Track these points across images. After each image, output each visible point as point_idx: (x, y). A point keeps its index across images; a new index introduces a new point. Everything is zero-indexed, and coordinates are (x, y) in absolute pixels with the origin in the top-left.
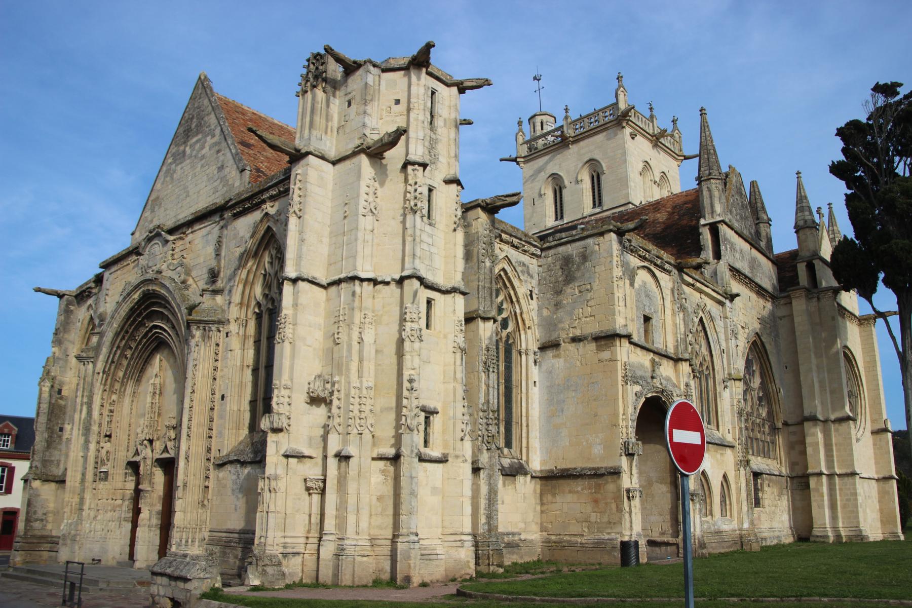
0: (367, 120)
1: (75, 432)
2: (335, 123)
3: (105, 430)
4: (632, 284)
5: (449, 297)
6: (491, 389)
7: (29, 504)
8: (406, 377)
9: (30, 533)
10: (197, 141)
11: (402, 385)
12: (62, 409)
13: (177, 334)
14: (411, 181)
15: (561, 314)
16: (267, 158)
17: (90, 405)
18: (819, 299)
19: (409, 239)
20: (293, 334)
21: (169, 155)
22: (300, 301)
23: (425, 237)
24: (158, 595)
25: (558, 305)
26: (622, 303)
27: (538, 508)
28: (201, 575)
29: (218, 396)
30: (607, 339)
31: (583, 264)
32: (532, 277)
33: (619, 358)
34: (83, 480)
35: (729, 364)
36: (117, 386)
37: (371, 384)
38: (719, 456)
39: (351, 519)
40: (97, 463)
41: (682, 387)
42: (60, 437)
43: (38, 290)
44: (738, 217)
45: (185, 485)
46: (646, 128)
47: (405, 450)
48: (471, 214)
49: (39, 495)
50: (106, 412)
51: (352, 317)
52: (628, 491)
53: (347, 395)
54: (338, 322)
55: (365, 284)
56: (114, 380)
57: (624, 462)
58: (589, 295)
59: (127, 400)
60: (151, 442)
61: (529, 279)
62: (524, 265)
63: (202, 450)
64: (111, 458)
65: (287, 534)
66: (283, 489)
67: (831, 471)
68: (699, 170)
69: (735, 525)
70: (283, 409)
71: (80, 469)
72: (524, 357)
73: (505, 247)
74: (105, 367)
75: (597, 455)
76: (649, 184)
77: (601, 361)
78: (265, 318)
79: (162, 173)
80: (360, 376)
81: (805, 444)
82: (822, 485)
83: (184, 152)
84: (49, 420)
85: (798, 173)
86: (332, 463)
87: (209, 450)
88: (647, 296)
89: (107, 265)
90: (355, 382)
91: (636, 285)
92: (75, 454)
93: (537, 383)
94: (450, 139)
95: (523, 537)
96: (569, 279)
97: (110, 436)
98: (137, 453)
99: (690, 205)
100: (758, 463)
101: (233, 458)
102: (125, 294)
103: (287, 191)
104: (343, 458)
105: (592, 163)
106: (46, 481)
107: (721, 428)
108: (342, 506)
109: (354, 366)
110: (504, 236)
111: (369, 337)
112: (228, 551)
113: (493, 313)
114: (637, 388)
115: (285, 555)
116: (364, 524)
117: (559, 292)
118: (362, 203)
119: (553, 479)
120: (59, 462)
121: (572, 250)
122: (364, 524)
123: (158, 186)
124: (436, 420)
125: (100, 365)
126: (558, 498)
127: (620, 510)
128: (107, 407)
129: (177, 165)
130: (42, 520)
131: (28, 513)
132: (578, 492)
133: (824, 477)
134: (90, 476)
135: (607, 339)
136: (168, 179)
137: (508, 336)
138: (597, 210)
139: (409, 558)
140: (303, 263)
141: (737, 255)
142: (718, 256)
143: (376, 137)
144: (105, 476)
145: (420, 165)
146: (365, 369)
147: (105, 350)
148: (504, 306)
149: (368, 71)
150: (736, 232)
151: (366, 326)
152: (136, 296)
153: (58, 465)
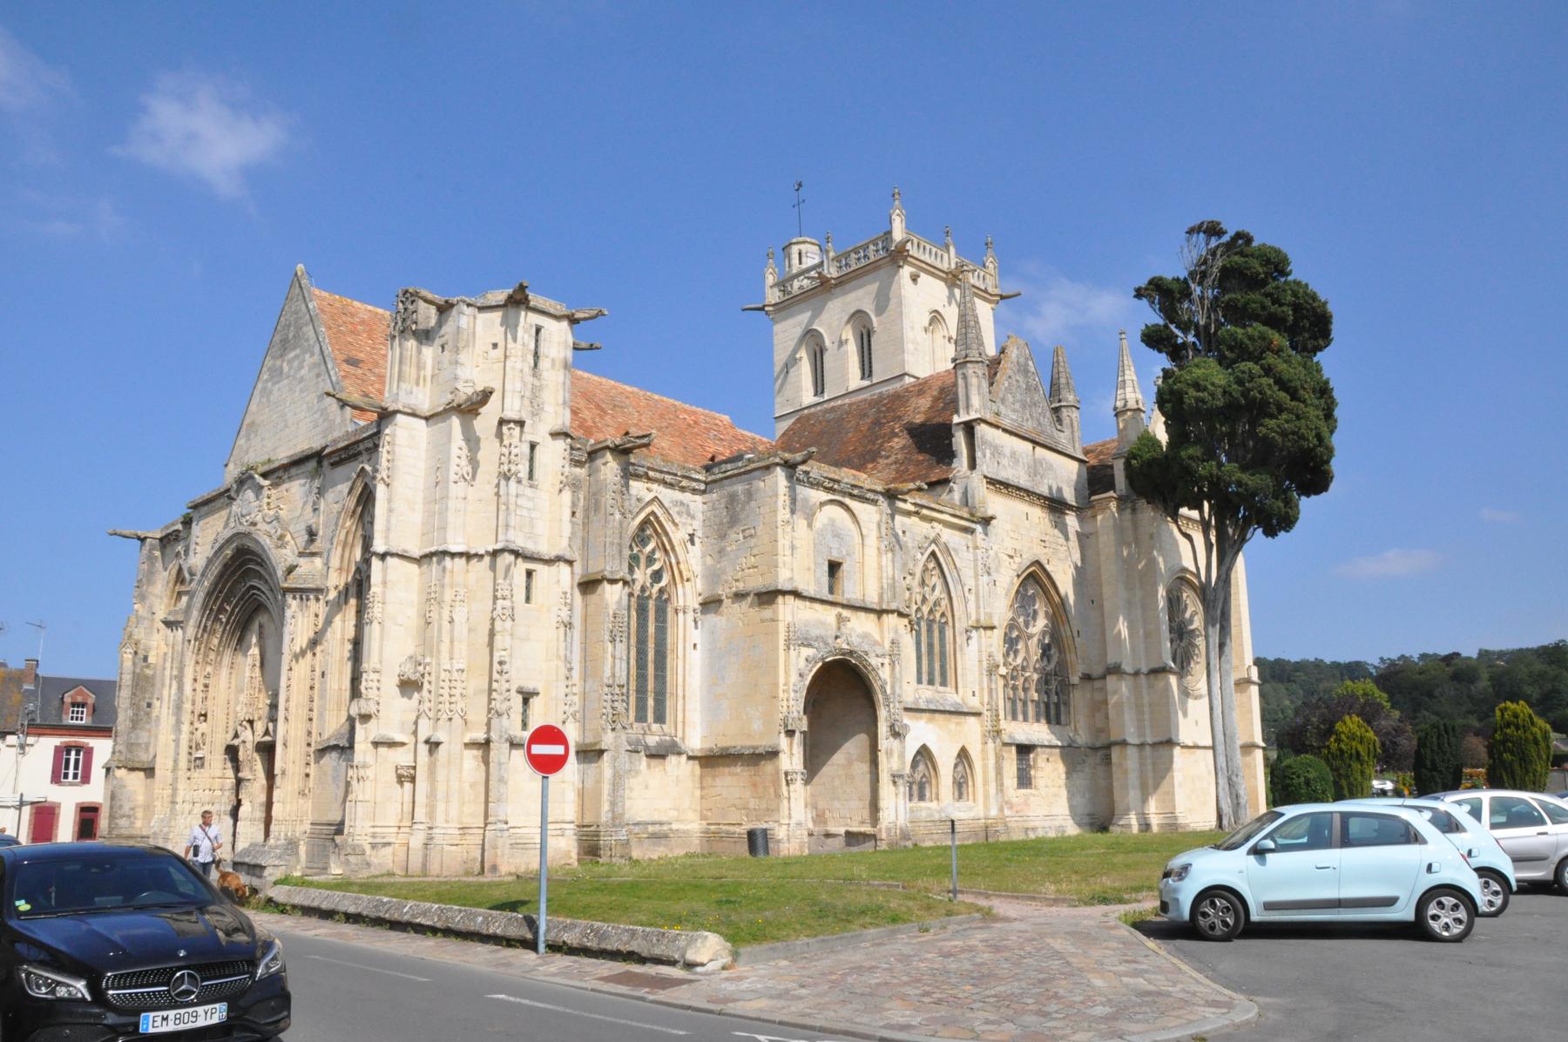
0: (459, 372)
1: (165, 711)
2: (429, 371)
3: (199, 709)
4: (810, 525)
5: (554, 569)
7: (113, 797)
8: (496, 659)
9: (115, 832)
10: (296, 357)
11: (495, 669)
12: (150, 680)
14: (506, 442)
15: (725, 563)
17: (180, 679)
19: (503, 507)
22: (389, 577)
25: (721, 552)
26: (788, 552)
27: (698, 793)
29: (318, 673)
30: (768, 597)
32: (693, 517)
33: (781, 617)
34: (175, 768)
36: (212, 656)
37: (461, 666)
41: (887, 645)
42: (148, 714)
44: (1017, 406)
45: (283, 773)
46: (938, 264)
47: (494, 736)
48: (599, 462)
50: (200, 687)
51: (442, 594)
52: (786, 774)
53: (438, 678)
54: (431, 599)
55: (457, 560)
57: (783, 742)
58: (753, 542)
59: (224, 671)
60: (251, 722)
61: (689, 521)
62: (682, 503)
63: (302, 734)
64: (208, 741)
66: (372, 777)
69: (979, 811)
70: (372, 694)
71: (172, 754)
72: (681, 615)
73: (655, 486)
75: (756, 735)
83: (281, 368)
84: (134, 694)
86: (423, 749)
87: (310, 733)
89: (195, 507)
92: (165, 740)
95: (674, 827)
96: (734, 521)
97: (205, 715)
98: (236, 736)
101: (333, 742)
102: (217, 546)
103: (376, 446)
104: (434, 746)
105: (858, 317)
106: (132, 769)
108: (432, 795)
110: (651, 474)
111: (459, 617)
113: (623, 572)
114: (810, 652)
115: (374, 846)
116: (454, 812)
117: (723, 536)
118: (454, 468)
119: (712, 760)
120: (147, 745)
121: (739, 488)
122: (454, 812)
124: (534, 701)
125: (191, 631)
126: (718, 782)
127: (778, 796)
128: (201, 681)
131: (111, 807)
134: (183, 763)
135: (768, 597)
137: (661, 591)
138: (866, 383)
139: (495, 847)
140: (392, 536)
141: (1005, 461)
142: (973, 465)
143: (470, 391)
144: (200, 763)
145: (516, 422)
146: (456, 650)
147: (195, 614)
148: (657, 555)
149: (461, 313)
150: (1005, 430)
152: (229, 552)
153: (147, 749)
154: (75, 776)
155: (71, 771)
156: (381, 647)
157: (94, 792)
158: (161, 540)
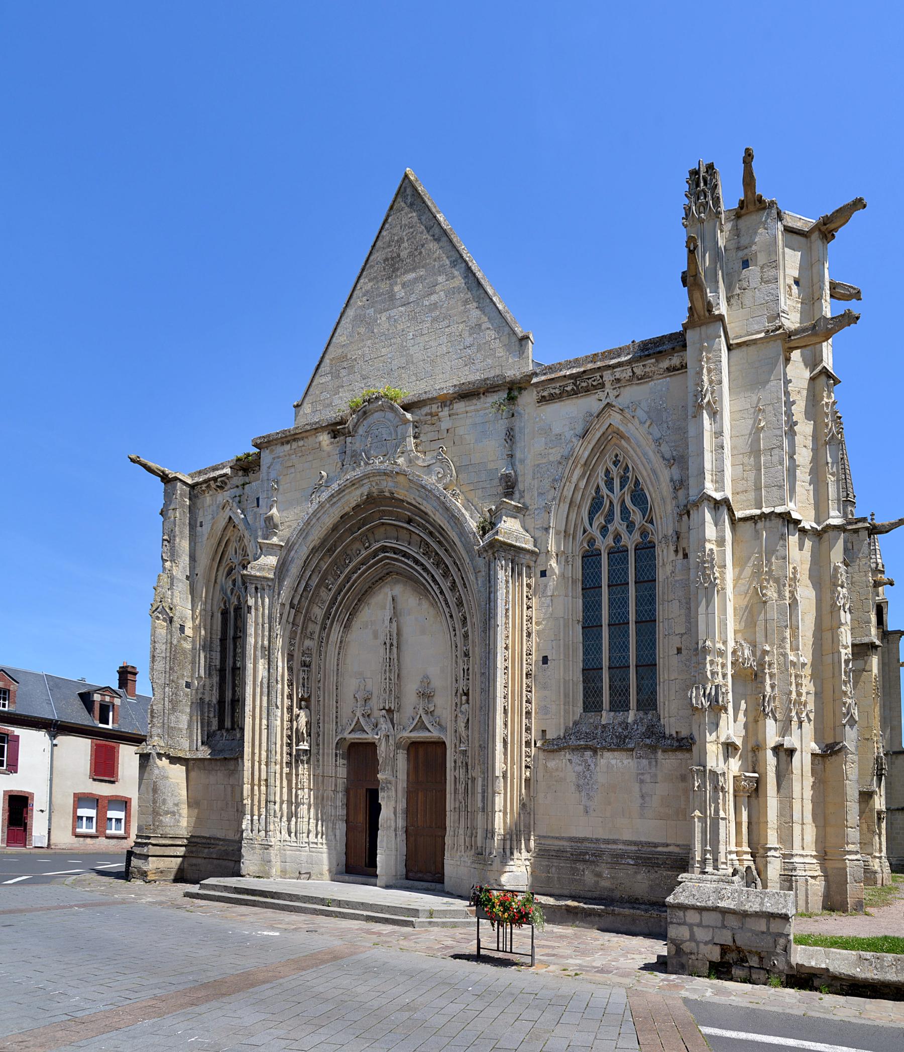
49: (167, 778)
89: (263, 444)
93: (198, 524)
100: (81, 812)
104: (785, 753)
112: (580, 866)
123: (341, 338)
130: (173, 814)
158: (192, 487)
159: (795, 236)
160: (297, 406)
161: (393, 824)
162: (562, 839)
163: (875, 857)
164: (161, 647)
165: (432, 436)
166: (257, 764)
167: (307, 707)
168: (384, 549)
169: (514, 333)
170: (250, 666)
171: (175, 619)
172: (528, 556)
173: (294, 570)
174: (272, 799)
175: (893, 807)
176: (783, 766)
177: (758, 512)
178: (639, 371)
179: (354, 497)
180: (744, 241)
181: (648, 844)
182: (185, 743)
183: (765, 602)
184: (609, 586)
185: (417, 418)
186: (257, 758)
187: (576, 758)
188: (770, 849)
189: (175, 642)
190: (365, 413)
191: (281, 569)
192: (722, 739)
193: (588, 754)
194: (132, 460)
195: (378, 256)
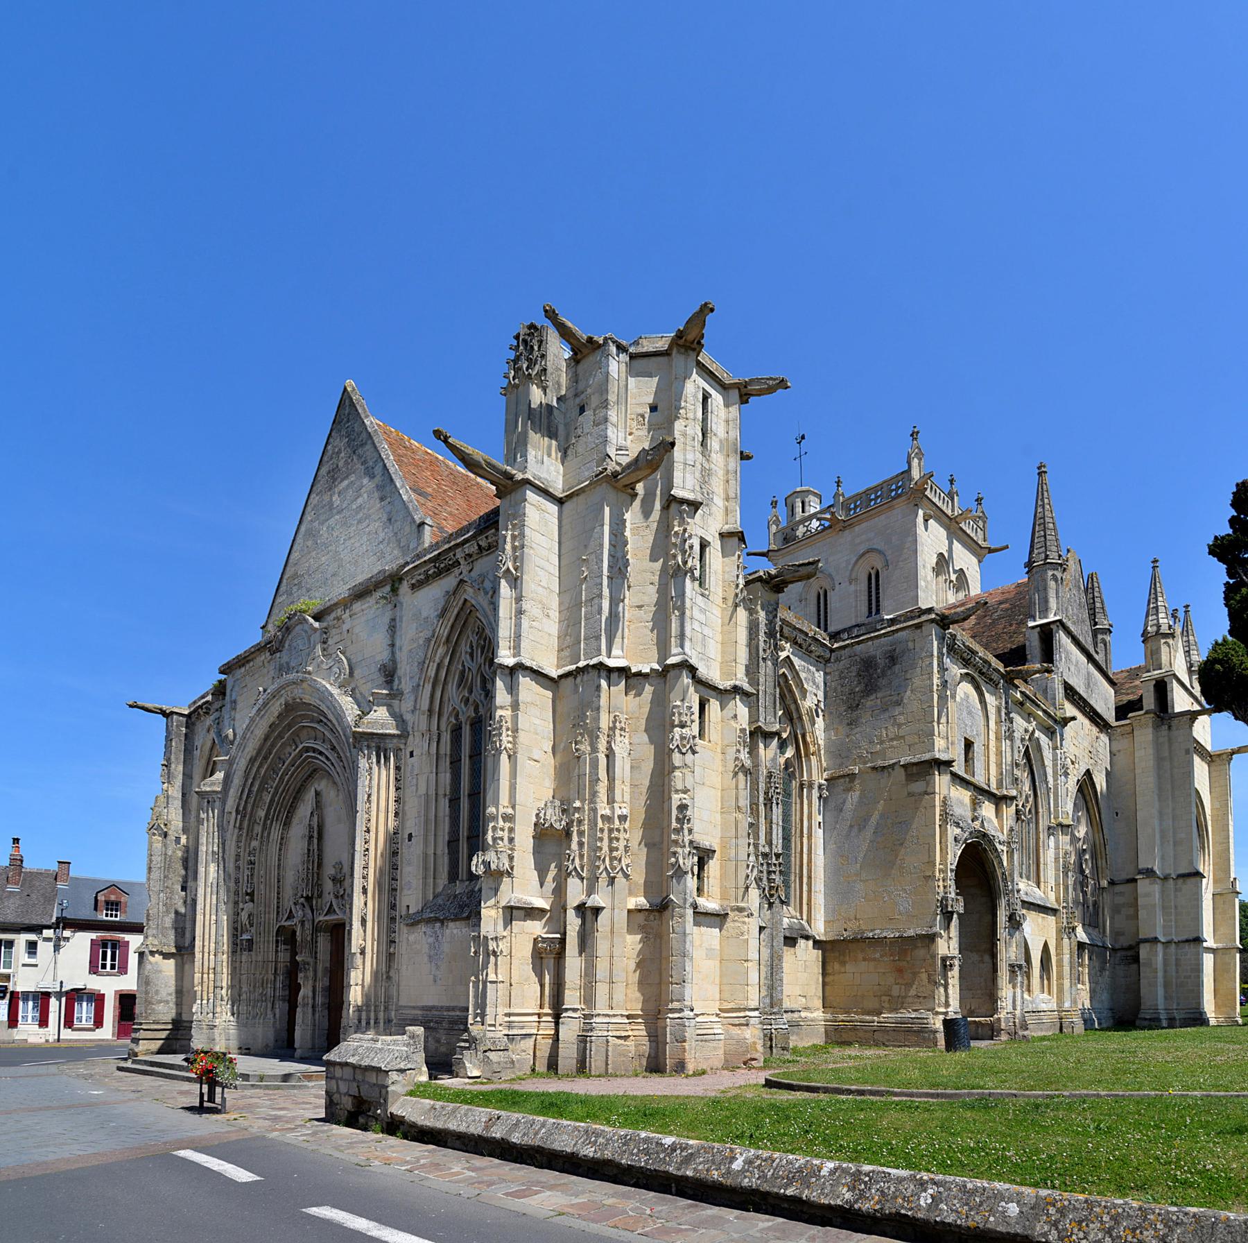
6: (774, 826)
13: (339, 757)
16: (450, 514)
18: (1170, 727)
20: (514, 743)
21: (309, 509)
23: (696, 614)
24: (338, 1091)
28: (402, 1066)
31: (890, 668)
35: (1056, 805)
37: (625, 811)
38: (1040, 920)
39: (601, 990)
40: (236, 929)
43: (1007, 547)
52: (944, 959)
56: (252, 823)
58: (897, 710)
65: (513, 1010)
67: (1169, 938)
68: (1031, 552)
74: (239, 805)
76: (942, 585)
77: (910, 795)
78: (466, 731)
79: (300, 536)
80: (611, 801)
81: (1137, 905)
82: (1156, 955)
83: (331, 503)
85: (1155, 561)
88: (970, 713)
89: (227, 669)
90: (604, 810)
91: (958, 699)
94: (728, 471)
95: (803, 1014)
96: (870, 688)
99: (1007, 605)
104: (588, 913)
107: (1042, 885)
109: (602, 788)
124: (713, 866)
126: (849, 967)
129: (322, 523)
132: (875, 959)
133: (1160, 945)
136: (309, 543)
151: (617, 732)
154: (113, 967)
155: (109, 962)
156: (513, 787)
157: (129, 982)
158: (189, 716)
159: (653, 359)
160: (263, 628)
161: (310, 1002)
162: (414, 1008)
163: (938, 1013)
164: (157, 859)
165: (337, 638)
166: (206, 955)
167: (252, 901)
168: (307, 749)
169: (414, 521)
170: (201, 870)
171: (170, 832)
172: (395, 741)
173: (237, 781)
174: (218, 984)
175: (1117, 947)
176: (588, 925)
177: (574, 667)
178: (483, 544)
179: (276, 708)
180: (581, 386)
181: (433, 1008)
182: (1052, 896)
183: (579, 757)
184: (470, 757)
185: (325, 624)
186: (206, 950)
187: (429, 930)
188: (567, 1010)
189: (170, 853)
190: (288, 629)
191: (227, 781)
192: (503, 903)
193: (438, 925)
194: (131, 706)
195: (324, 470)
